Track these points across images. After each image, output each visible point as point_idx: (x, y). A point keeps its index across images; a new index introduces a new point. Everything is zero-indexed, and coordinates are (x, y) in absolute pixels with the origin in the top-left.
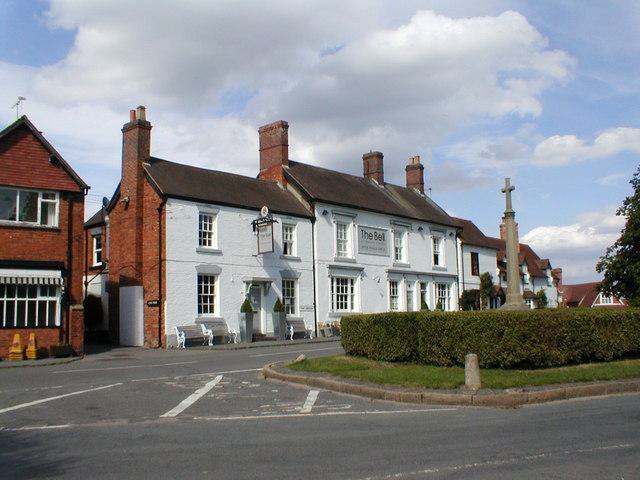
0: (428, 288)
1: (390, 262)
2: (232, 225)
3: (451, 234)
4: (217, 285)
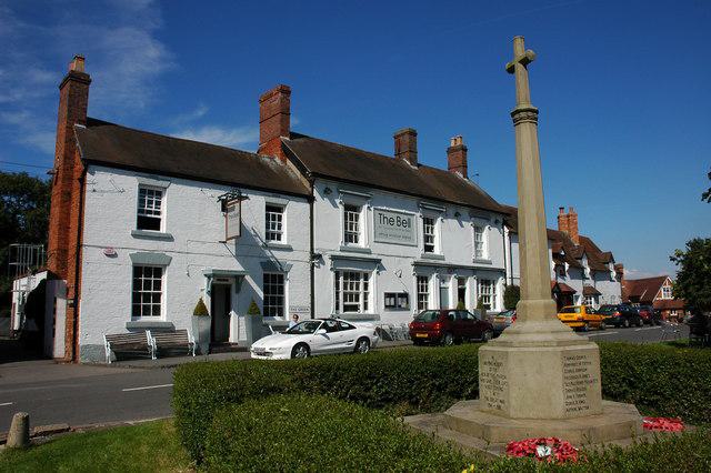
0: (467, 285)
1: (418, 253)
2: (190, 209)
3: (496, 222)
4: (164, 279)
